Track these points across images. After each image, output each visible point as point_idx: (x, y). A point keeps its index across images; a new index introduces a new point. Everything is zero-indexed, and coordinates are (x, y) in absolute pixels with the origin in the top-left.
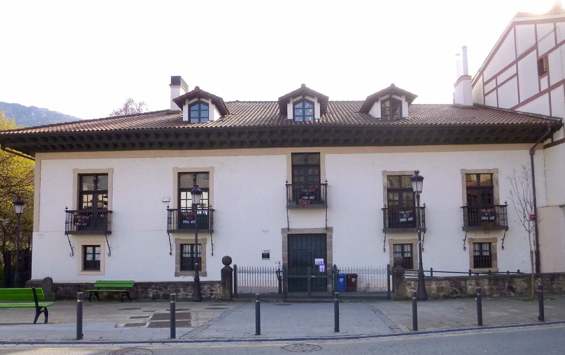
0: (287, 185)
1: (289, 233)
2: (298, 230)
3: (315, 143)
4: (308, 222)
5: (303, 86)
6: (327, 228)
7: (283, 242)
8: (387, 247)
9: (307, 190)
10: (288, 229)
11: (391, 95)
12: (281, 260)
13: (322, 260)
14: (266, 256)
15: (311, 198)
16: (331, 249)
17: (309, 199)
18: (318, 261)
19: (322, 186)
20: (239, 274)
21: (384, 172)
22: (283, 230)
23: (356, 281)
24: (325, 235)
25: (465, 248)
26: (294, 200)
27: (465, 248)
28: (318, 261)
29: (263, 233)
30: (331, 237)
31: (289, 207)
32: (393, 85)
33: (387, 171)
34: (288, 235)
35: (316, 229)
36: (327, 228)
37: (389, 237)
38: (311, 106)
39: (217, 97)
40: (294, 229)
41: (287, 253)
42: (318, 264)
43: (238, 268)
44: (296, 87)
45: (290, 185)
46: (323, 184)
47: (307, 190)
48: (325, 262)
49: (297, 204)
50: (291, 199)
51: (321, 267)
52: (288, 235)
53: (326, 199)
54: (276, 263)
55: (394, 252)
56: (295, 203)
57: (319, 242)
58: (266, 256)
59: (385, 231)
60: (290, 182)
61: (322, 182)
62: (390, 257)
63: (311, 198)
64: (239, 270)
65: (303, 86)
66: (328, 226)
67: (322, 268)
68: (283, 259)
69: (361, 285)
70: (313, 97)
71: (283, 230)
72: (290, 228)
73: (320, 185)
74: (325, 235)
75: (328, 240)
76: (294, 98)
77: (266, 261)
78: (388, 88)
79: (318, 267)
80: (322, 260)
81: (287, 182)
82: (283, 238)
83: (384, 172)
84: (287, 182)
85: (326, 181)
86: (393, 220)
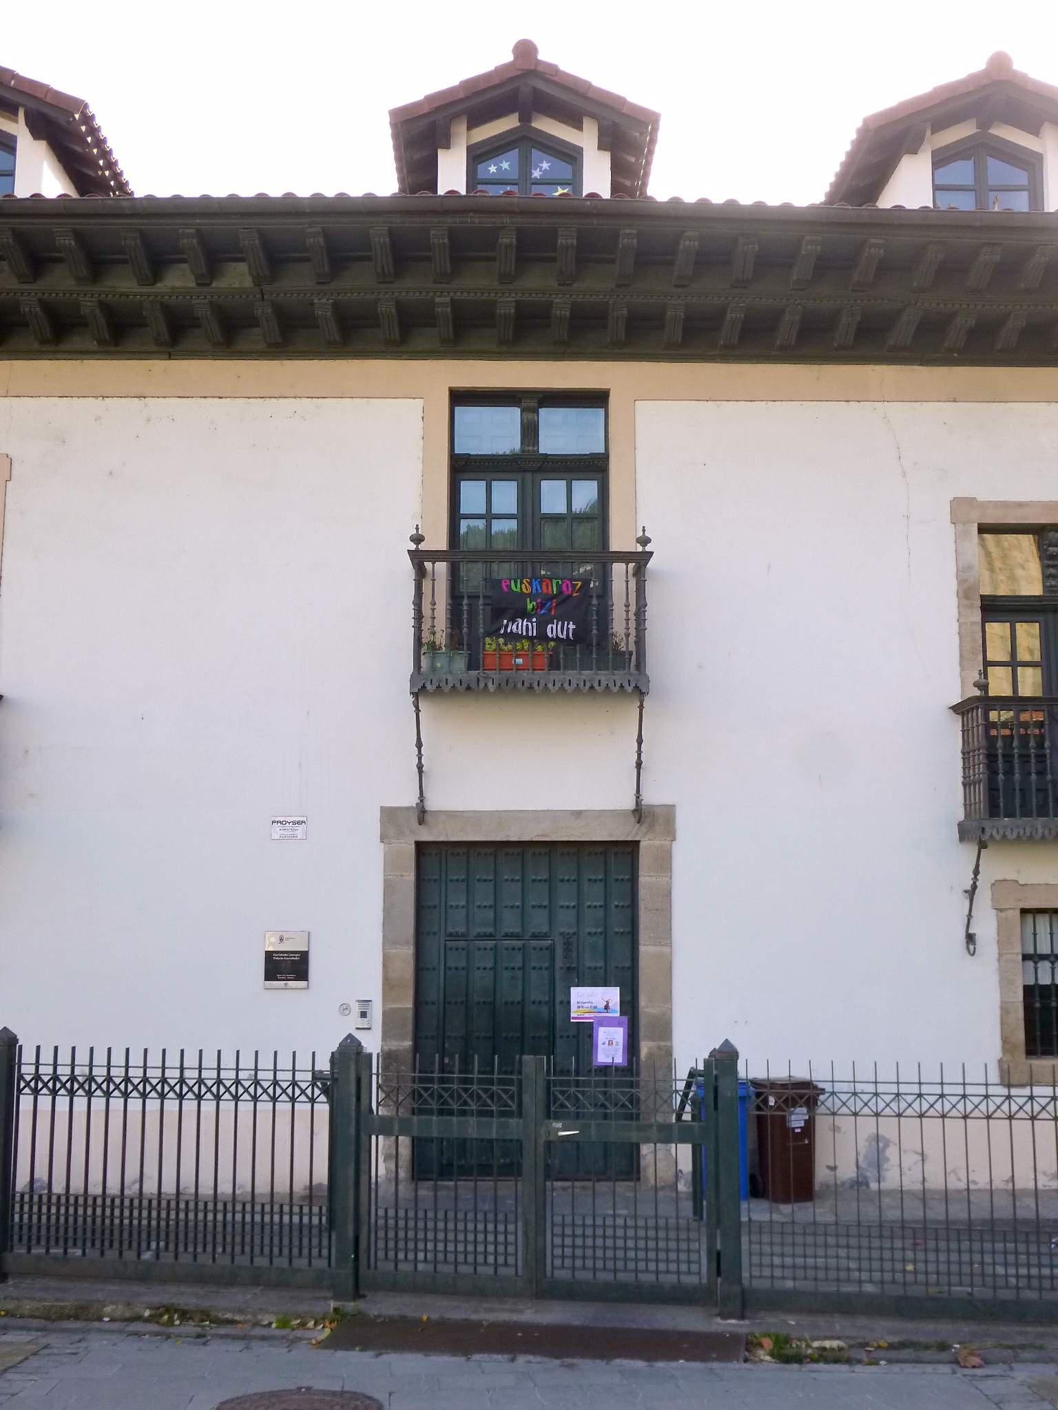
0: (419, 559)
1: (426, 836)
2: (476, 817)
3: (585, 333)
4: (533, 772)
5: (525, 50)
6: (640, 813)
7: (389, 888)
8: (986, 927)
9: (531, 607)
10: (422, 814)
11: (984, 125)
12: (375, 993)
13: (612, 995)
14: (287, 967)
15: (553, 630)
16: (665, 935)
17: (542, 637)
18: (590, 1000)
19: (618, 569)
20: (26, 1102)
21: (960, 506)
22: (389, 815)
23: (809, 1128)
24: (630, 849)
25: (970, 938)
26: (455, 641)
27: (970, 938)
28: (590, 1000)
29: (277, 831)
30: (665, 862)
31: (424, 688)
32: (999, 62)
33: (981, 498)
34: (421, 847)
35: (578, 814)
36: (640, 813)
37: (1003, 866)
38: (565, 171)
39: (58, 94)
40: (452, 815)
41: (409, 951)
42: (588, 1017)
43: (28, 1056)
44: (487, 56)
45: (435, 556)
46: (624, 557)
47: (531, 607)
48: (630, 1006)
49: (472, 665)
50: (441, 638)
51: (603, 1034)
52: (421, 847)
53: (640, 642)
54: (345, 1009)
55: (1026, 957)
56: (460, 663)
57: (592, 890)
58: (287, 967)
59: (974, 833)
60: (438, 540)
61: (620, 541)
62: (1005, 982)
63: (553, 630)
64: (28, 1070)
65: (525, 50)
66: (651, 797)
67: (609, 1046)
68: (389, 985)
69: (838, 1153)
70: (574, 119)
71: (389, 815)
72: (432, 804)
73: (605, 558)
74: (630, 849)
75: (644, 879)
76: (475, 120)
77: (288, 993)
78: (973, 78)
79: (585, 1033)
80: (612, 995)
81: (417, 539)
82: (390, 863)
83: (960, 506)
84: (417, 539)
85: (645, 541)
86: (1009, 772)
